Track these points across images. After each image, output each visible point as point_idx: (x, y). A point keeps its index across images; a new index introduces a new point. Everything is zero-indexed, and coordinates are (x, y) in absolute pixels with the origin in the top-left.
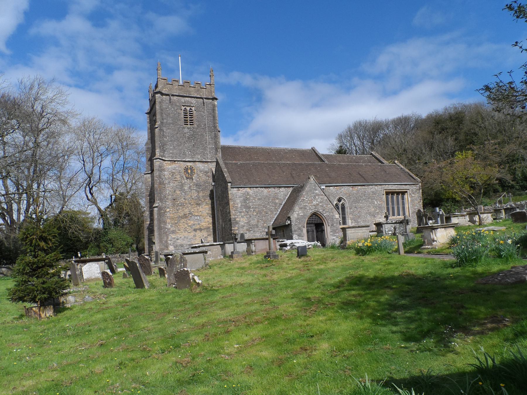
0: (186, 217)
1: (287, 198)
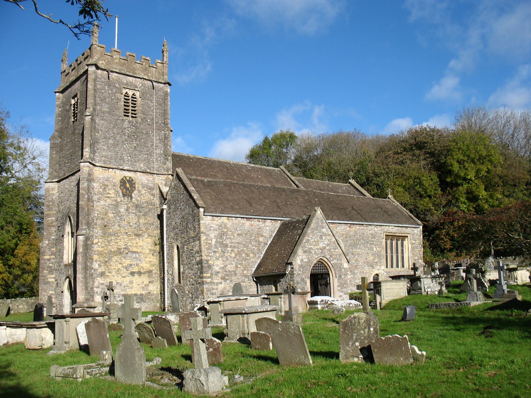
0: (121, 253)
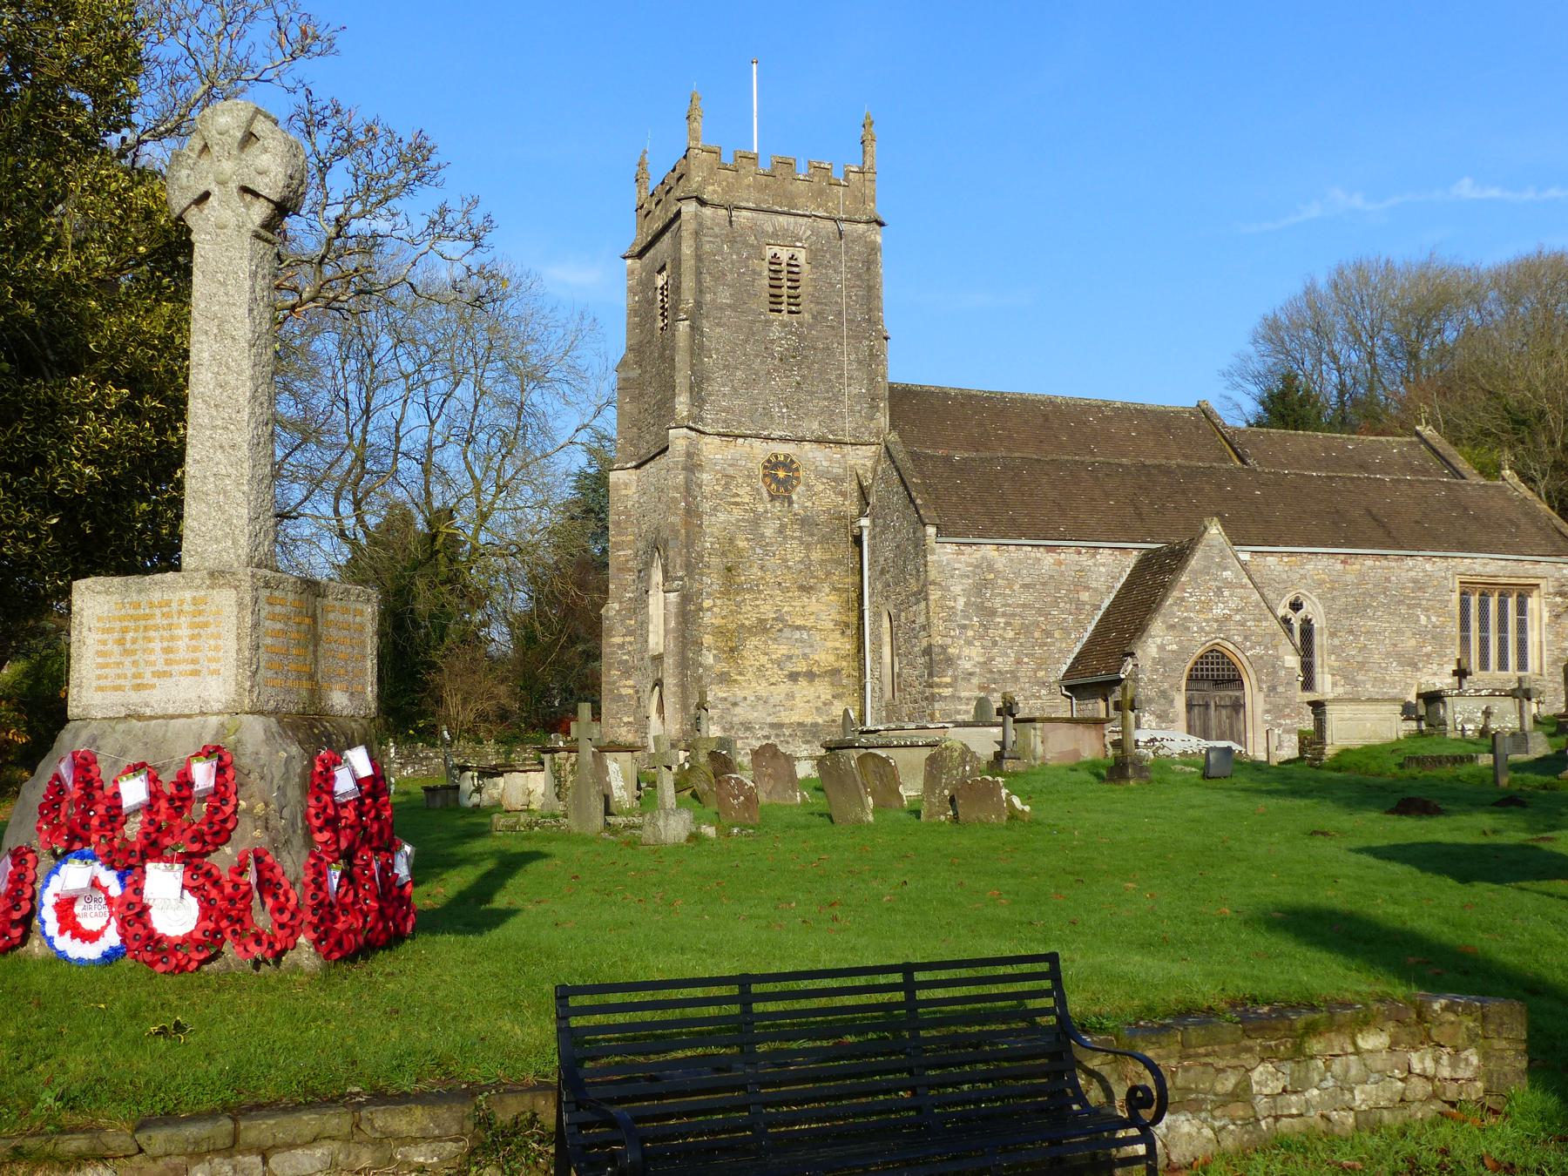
0: (765, 630)
1: (1119, 585)
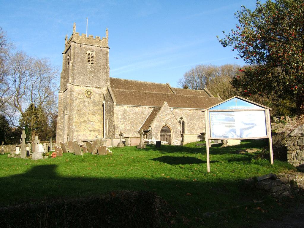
1: (150, 114)
